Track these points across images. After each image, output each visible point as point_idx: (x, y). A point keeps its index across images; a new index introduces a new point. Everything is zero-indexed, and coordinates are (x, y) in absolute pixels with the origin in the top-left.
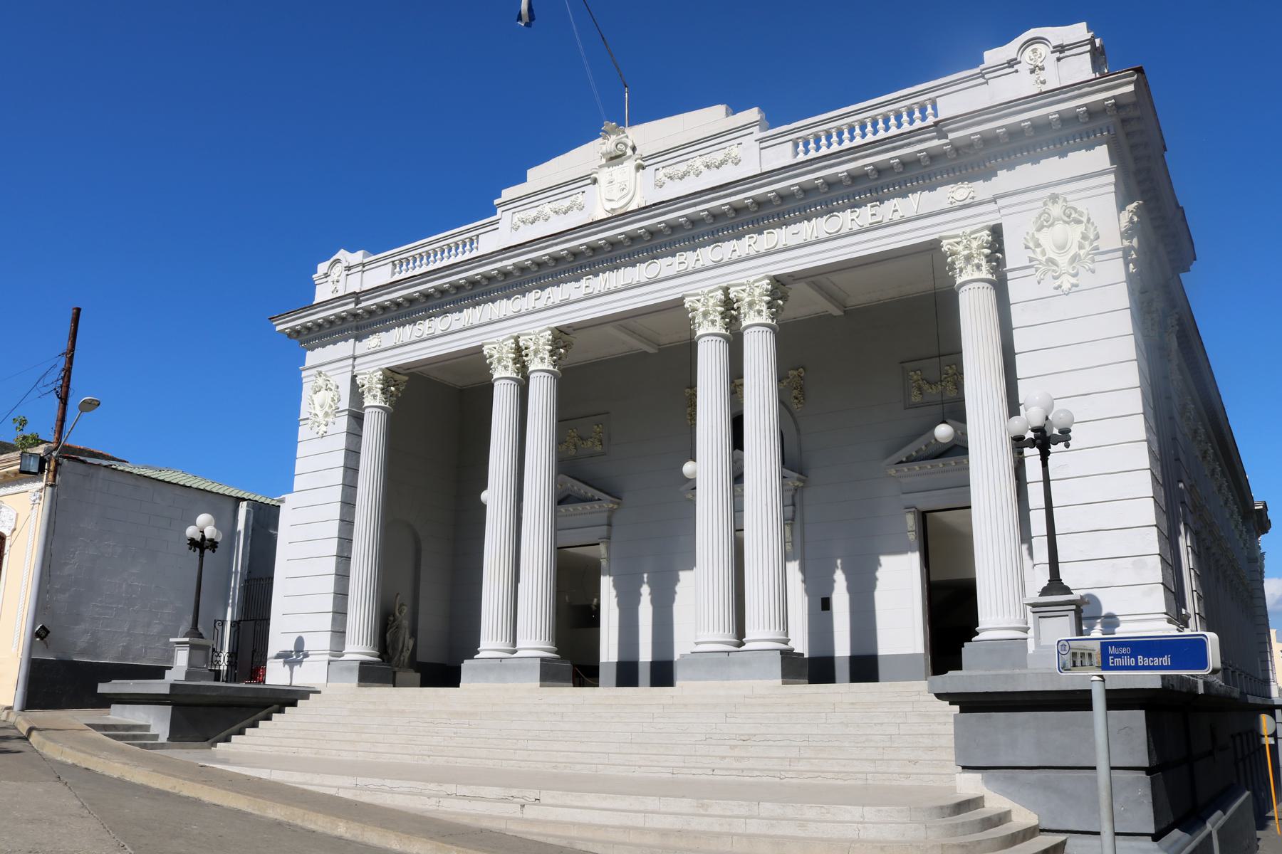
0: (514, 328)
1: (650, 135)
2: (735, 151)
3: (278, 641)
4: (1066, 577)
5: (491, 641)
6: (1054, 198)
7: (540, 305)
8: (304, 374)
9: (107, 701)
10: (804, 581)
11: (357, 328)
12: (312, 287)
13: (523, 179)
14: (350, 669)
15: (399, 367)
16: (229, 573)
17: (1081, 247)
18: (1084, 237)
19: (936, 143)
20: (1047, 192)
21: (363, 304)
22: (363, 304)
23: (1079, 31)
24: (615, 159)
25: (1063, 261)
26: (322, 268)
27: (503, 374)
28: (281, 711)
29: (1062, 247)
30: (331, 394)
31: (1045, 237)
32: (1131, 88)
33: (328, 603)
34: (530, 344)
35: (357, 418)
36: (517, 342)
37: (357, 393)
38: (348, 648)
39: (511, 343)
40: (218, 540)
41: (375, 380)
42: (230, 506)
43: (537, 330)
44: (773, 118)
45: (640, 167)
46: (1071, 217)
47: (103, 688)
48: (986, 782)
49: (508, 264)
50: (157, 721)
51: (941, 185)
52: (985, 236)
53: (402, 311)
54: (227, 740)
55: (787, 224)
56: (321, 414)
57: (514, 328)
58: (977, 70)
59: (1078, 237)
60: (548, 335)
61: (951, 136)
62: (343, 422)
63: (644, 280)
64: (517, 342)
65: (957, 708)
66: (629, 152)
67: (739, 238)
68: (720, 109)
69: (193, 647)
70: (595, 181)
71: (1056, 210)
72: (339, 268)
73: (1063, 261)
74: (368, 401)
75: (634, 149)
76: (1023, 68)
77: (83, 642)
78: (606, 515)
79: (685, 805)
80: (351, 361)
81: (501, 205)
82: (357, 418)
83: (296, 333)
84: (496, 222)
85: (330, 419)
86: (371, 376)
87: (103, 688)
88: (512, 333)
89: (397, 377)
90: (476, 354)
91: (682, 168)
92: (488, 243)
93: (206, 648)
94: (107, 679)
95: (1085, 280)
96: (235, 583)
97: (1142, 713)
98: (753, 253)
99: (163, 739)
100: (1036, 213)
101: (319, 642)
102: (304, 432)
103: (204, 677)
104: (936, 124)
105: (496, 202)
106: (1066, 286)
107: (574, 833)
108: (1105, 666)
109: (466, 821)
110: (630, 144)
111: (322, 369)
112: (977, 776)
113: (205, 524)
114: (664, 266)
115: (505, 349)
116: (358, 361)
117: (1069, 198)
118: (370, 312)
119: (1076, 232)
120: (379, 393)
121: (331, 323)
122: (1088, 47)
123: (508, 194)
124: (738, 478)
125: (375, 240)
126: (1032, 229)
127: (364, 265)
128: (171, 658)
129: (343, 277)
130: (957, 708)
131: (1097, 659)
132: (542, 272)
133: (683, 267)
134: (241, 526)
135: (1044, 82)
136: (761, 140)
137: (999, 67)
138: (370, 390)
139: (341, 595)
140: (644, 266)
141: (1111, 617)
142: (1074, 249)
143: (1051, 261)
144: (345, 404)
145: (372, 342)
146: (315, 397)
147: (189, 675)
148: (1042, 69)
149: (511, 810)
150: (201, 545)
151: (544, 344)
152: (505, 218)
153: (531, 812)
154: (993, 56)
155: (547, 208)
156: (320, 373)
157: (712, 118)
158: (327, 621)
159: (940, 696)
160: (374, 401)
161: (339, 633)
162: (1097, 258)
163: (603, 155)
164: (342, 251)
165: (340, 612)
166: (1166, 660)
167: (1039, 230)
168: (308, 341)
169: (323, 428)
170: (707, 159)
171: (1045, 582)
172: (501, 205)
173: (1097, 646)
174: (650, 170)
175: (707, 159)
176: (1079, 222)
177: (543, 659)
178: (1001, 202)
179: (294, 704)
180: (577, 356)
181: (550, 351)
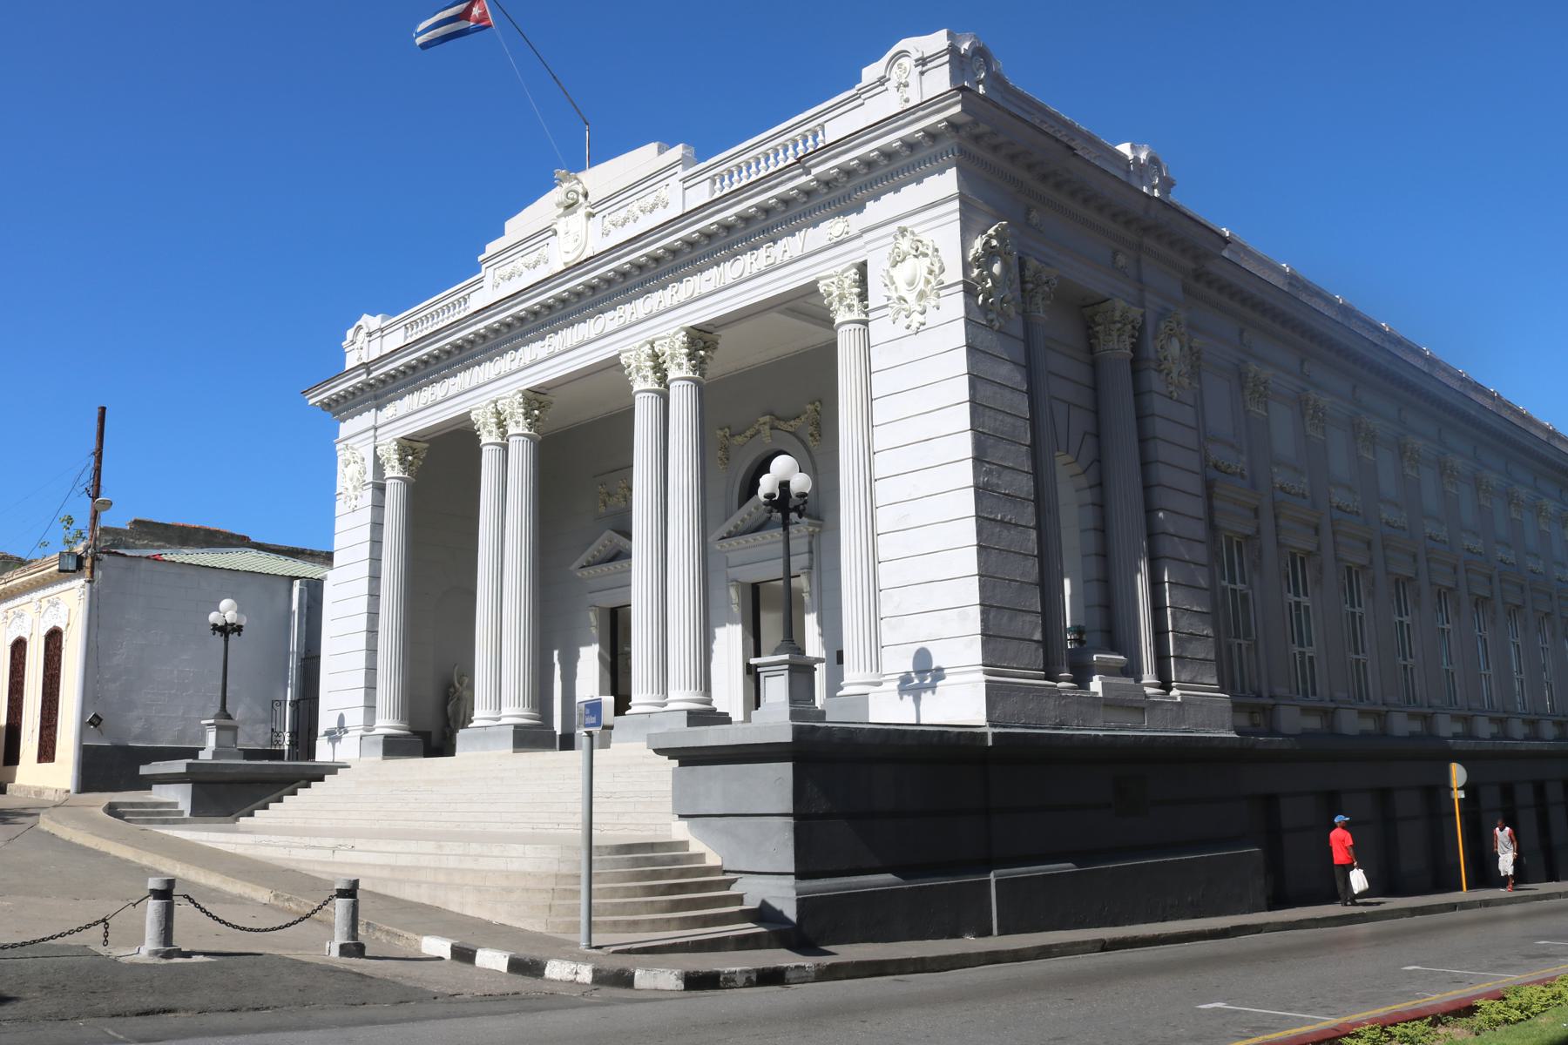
0: (649, 336)
1: (600, 178)
2: (664, 193)
3: (326, 721)
5: (481, 713)
6: (903, 231)
7: (515, 366)
8: (338, 447)
9: (146, 783)
10: (822, 635)
11: (376, 398)
12: (342, 355)
13: (501, 233)
14: (376, 743)
15: (414, 434)
16: (288, 653)
17: (928, 282)
18: (931, 272)
19: (804, 179)
20: (894, 227)
21: (374, 374)
22: (374, 374)
23: (938, 41)
24: (570, 207)
26: (350, 333)
28: (308, 786)
30: (926, 262)
32: (958, 109)
33: (360, 679)
34: (833, 289)
35: (379, 488)
37: (378, 467)
38: (379, 722)
39: (647, 349)
40: (243, 623)
41: (678, 344)
42: (284, 585)
43: (839, 269)
44: (702, 149)
45: (590, 215)
47: (144, 770)
48: (690, 827)
49: (729, 214)
50: (179, 796)
51: (906, 184)
52: (853, 274)
53: (615, 289)
54: (251, 814)
55: (701, 271)
56: (911, 297)
57: (492, 392)
58: (853, 92)
59: (925, 272)
60: (394, 446)
61: (815, 171)
62: (368, 494)
63: (593, 336)
65: (675, 763)
66: (581, 199)
67: (664, 288)
68: (653, 147)
69: (219, 728)
70: (555, 233)
71: (905, 244)
72: (362, 334)
74: (389, 473)
75: (586, 196)
76: (890, 85)
77: (137, 727)
78: (806, 540)
79: (429, 847)
81: (486, 261)
82: (379, 488)
83: (327, 406)
84: (480, 280)
85: (933, 301)
87: (144, 770)
88: (489, 396)
89: (416, 445)
90: (613, 365)
91: (623, 213)
92: (477, 302)
93: (1263, 709)
94: (147, 762)
95: (932, 317)
96: (293, 663)
97: (789, 765)
98: (675, 303)
99: (187, 815)
100: (889, 249)
101: (355, 719)
102: (340, 507)
103: (231, 756)
104: (799, 160)
105: (480, 258)
106: (915, 325)
107: (318, 868)
109: (276, 863)
110: (581, 191)
111: (903, 223)
112: (684, 823)
113: (227, 611)
114: (792, 245)
115: (847, 282)
117: (916, 230)
120: (397, 464)
121: (564, 301)
122: (947, 58)
123: (492, 248)
125: (391, 304)
126: (887, 265)
127: (382, 330)
128: (203, 737)
129: (371, 341)
130: (675, 763)
132: (679, 261)
133: (771, 261)
134: (295, 606)
135: (907, 101)
136: (684, 180)
137: (872, 87)
138: (638, 370)
139: (371, 669)
140: (728, 264)
141: (940, 669)
142: (921, 286)
143: (902, 299)
144: (369, 478)
145: (389, 411)
146: (893, 272)
147: (216, 754)
148: (906, 85)
149: (325, 855)
150: (225, 630)
151: (851, 287)
152: (489, 274)
153: (340, 856)
154: (870, 73)
155: (520, 263)
156: (903, 231)
157: (645, 158)
158: (359, 697)
159: (658, 751)
160: (393, 471)
161: (370, 707)
162: (942, 293)
163: (558, 205)
164: (365, 317)
165: (371, 688)
168: (338, 413)
169: (917, 319)
170: (642, 203)
172: (486, 261)
175: (642, 203)
176: (926, 255)
177: (516, 726)
178: (867, 237)
179: (322, 779)
180: (723, 362)
181: (688, 355)
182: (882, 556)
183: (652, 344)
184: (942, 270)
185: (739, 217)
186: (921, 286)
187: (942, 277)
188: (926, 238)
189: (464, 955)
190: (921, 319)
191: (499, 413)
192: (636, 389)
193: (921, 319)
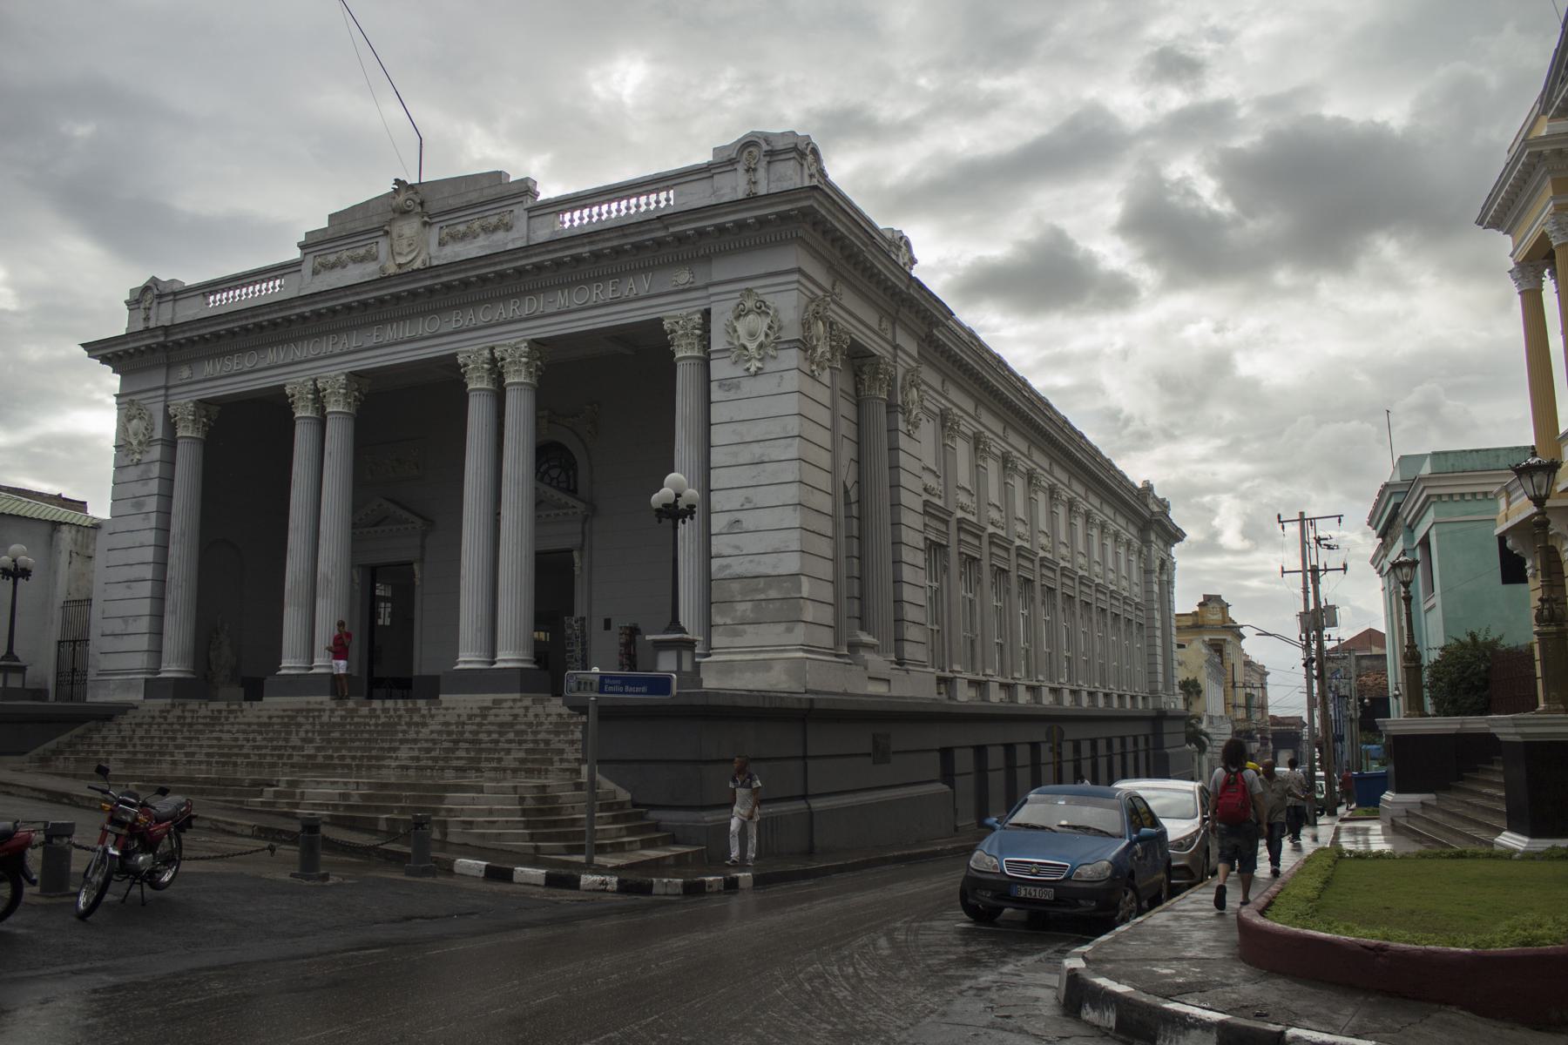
0: (490, 342)
4: (16, 652)
17: (767, 335)
18: (770, 328)
25: (752, 346)
27: (477, 383)
29: (752, 335)
31: (741, 327)
35: (170, 443)
36: (492, 354)
39: (486, 353)
46: (762, 309)
49: (306, 310)
52: (697, 318)
59: (765, 328)
61: (671, 230)
62: (156, 452)
64: (492, 354)
73: (752, 346)
76: (741, 168)
80: (162, 392)
82: (170, 443)
86: (183, 401)
100: (733, 304)
106: (753, 369)
108: (601, 691)
111: (749, 285)
116: (171, 391)
118: (177, 343)
119: (761, 324)
124: (497, 515)
126: (730, 315)
131: (596, 686)
166: (644, 689)
167: (738, 317)
169: (754, 365)
170: (484, 222)
171: (667, 624)
173: (597, 678)
174: (436, 229)
178: (712, 290)
182: (714, 551)
183: (315, 381)
184: (780, 328)
185: (328, 309)
186: (762, 338)
187: (782, 334)
188: (769, 299)
189: (498, 874)
190: (759, 365)
191: (316, 391)
192: (679, 355)
193: (759, 365)
